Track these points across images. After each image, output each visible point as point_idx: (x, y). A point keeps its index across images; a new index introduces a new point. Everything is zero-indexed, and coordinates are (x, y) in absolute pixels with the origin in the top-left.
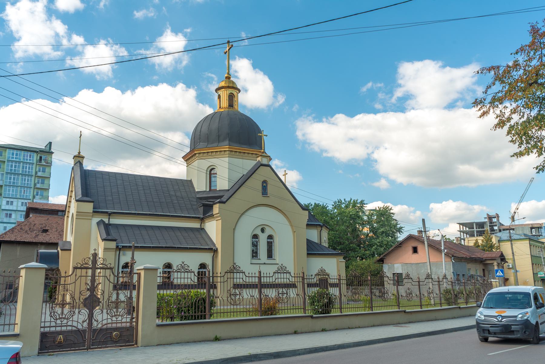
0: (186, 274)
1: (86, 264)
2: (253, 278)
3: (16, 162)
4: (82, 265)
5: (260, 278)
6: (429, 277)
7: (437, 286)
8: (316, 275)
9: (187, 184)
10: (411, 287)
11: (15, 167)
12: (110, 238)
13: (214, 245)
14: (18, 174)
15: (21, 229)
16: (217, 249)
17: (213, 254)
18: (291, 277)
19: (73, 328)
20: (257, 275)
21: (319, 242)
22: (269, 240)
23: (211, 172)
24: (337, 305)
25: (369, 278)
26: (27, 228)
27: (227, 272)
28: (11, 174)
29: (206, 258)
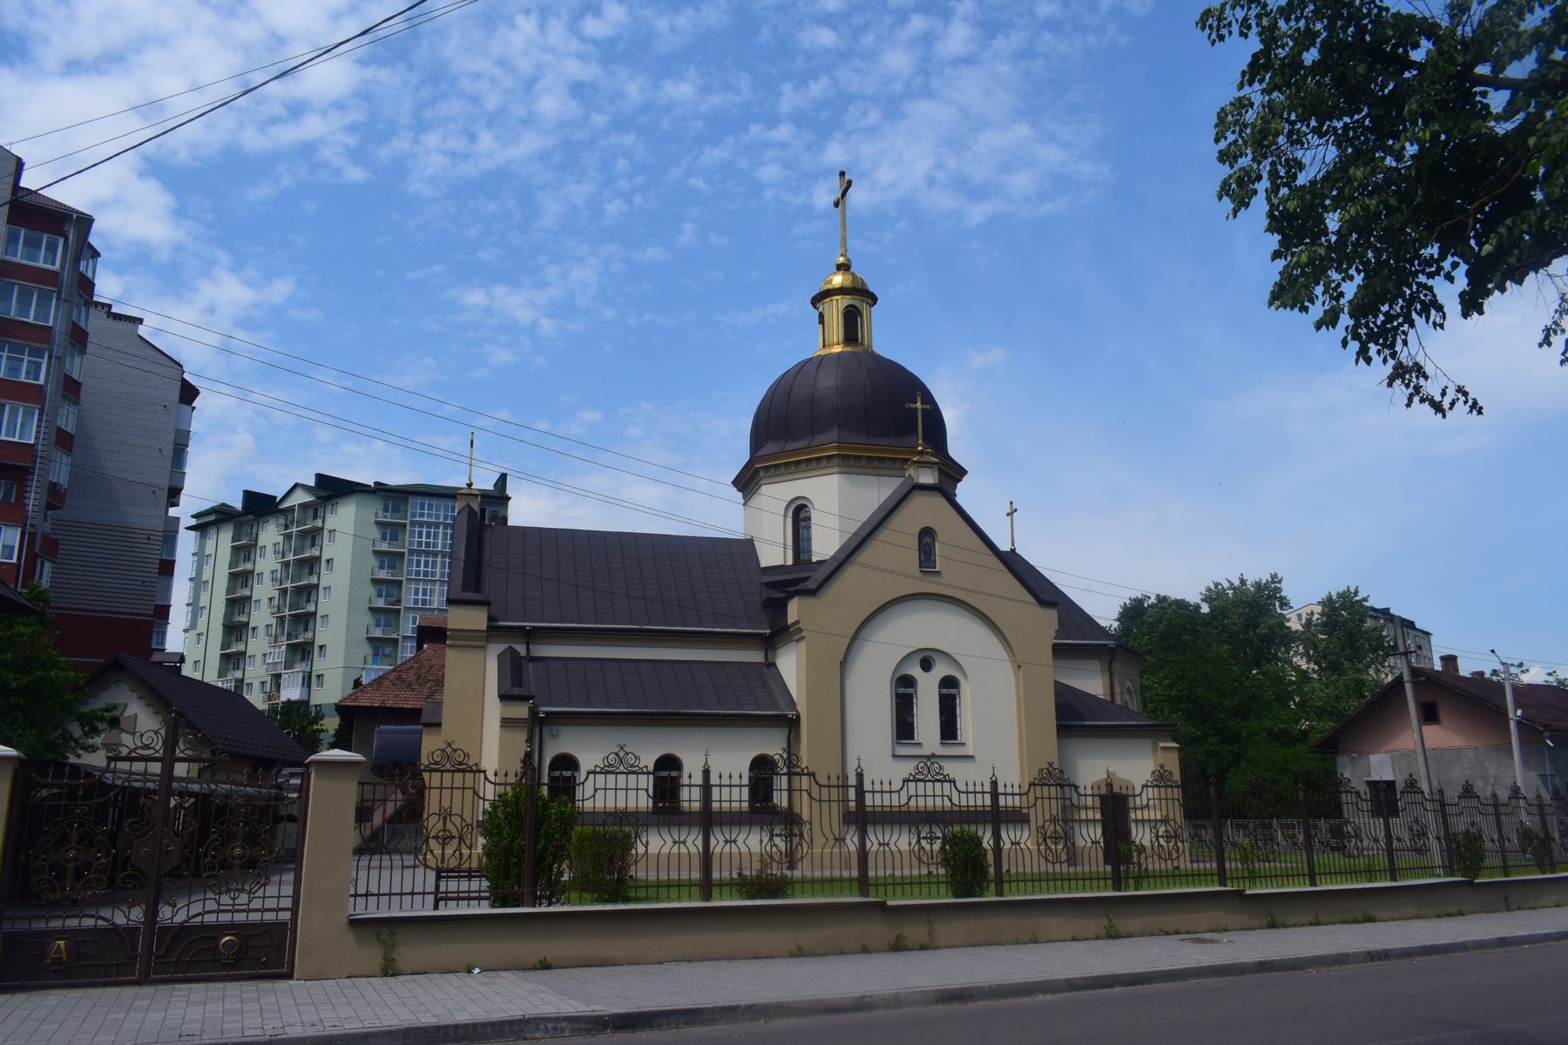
0: (458, 776)
1: (147, 747)
2: (886, 796)
3: (429, 525)
4: (134, 750)
5: (995, 794)
6: (1468, 791)
7: (1492, 819)
8: (906, 781)
9: (746, 548)
10: (1479, 818)
11: (428, 536)
12: (517, 691)
13: (793, 704)
14: (435, 554)
15: (399, 678)
16: (798, 717)
17: (786, 731)
18: (955, 793)
19: (100, 922)
20: (987, 788)
21: (1108, 698)
22: (945, 691)
23: (800, 514)
24: (1491, 860)
25: (1301, 794)
26: (412, 676)
27: (594, 773)
28: (419, 553)
29: (773, 745)
